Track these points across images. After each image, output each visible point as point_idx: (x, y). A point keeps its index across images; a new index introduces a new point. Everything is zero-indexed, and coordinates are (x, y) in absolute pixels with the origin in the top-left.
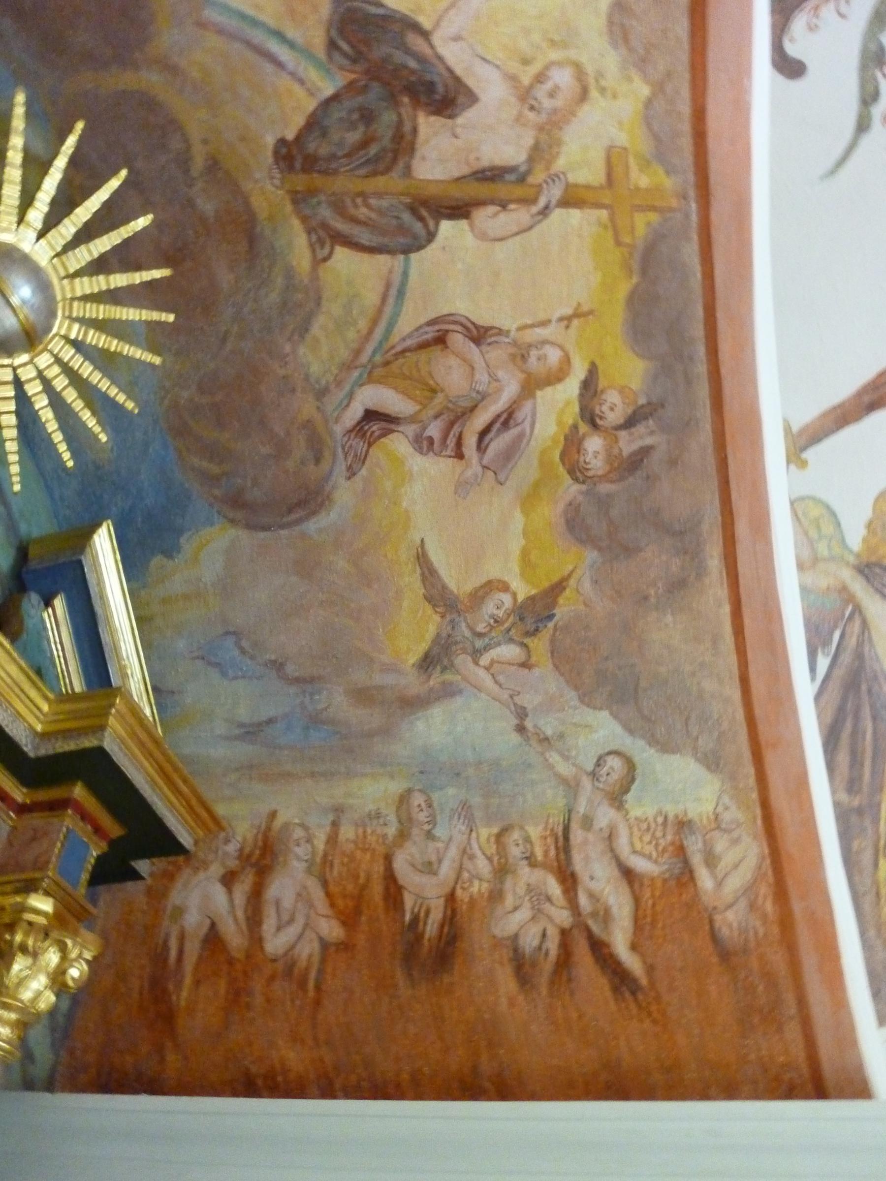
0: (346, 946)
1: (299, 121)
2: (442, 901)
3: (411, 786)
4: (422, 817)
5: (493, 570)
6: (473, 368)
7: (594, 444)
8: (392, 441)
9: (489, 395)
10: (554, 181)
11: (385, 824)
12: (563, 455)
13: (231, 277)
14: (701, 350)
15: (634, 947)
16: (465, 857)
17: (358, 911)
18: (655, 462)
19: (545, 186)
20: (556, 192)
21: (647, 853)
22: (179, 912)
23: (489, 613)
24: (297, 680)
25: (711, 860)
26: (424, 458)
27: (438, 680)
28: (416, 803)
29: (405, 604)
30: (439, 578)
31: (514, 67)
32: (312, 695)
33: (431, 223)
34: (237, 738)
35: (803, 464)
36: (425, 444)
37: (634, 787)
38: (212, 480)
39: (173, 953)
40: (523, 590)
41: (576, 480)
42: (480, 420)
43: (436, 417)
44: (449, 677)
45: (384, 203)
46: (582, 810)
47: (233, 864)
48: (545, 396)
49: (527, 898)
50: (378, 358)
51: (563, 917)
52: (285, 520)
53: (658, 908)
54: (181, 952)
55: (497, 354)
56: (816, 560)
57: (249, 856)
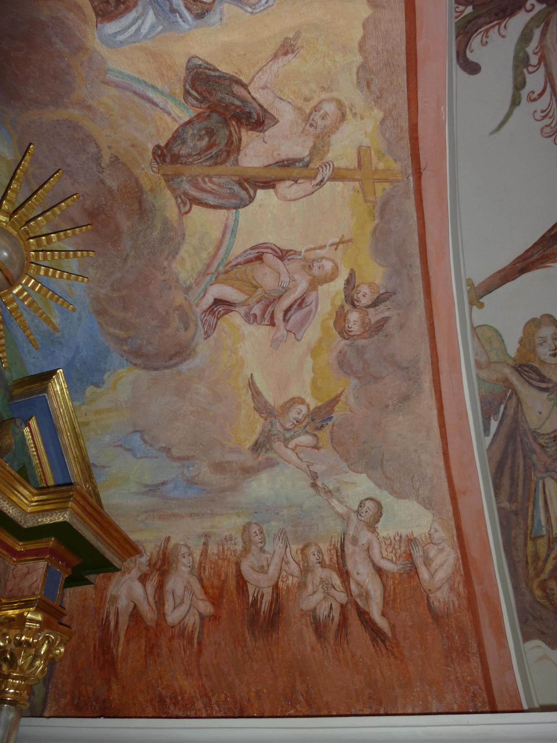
0: (215, 617)
1: (168, 135)
2: (271, 589)
3: (250, 520)
4: (257, 539)
5: (294, 391)
6: (280, 274)
7: (354, 316)
8: (231, 316)
9: (290, 289)
10: (326, 166)
11: (235, 544)
12: (335, 323)
13: (129, 224)
14: (417, 261)
15: (383, 614)
16: (284, 562)
17: (221, 596)
18: (391, 327)
19: (321, 169)
20: (328, 172)
21: (390, 558)
22: (115, 599)
23: (294, 417)
24: (179, 459)
25: (427, 562)
26: (252, 326)
27: (264, 457)
28: (253, 531)
29: (243, 412)
30: (263, 397)
31: (300, 103)
32: (188, 467)
33: (252, 192)
34: (143, 494)
35: (481, 306)
36: (252, 318)
37: (382, 519)
38: (122, 341)
39: (112, 624)
40: (313, 403)
41: (344, 338)
42: (285, 303)
43: (258, 302)
44: (271, 455)
45: (222, 181)
46: (351, 534)
47: (145, 569)
48: (323, 289)
49: (321, 586)
50: (221, 269)
51: (342, 597)
52: (167, 364)
53: (397, 590)
54: (117, 623)
55: (294, 266)
56: (489, 363)
57: (155, 564)
